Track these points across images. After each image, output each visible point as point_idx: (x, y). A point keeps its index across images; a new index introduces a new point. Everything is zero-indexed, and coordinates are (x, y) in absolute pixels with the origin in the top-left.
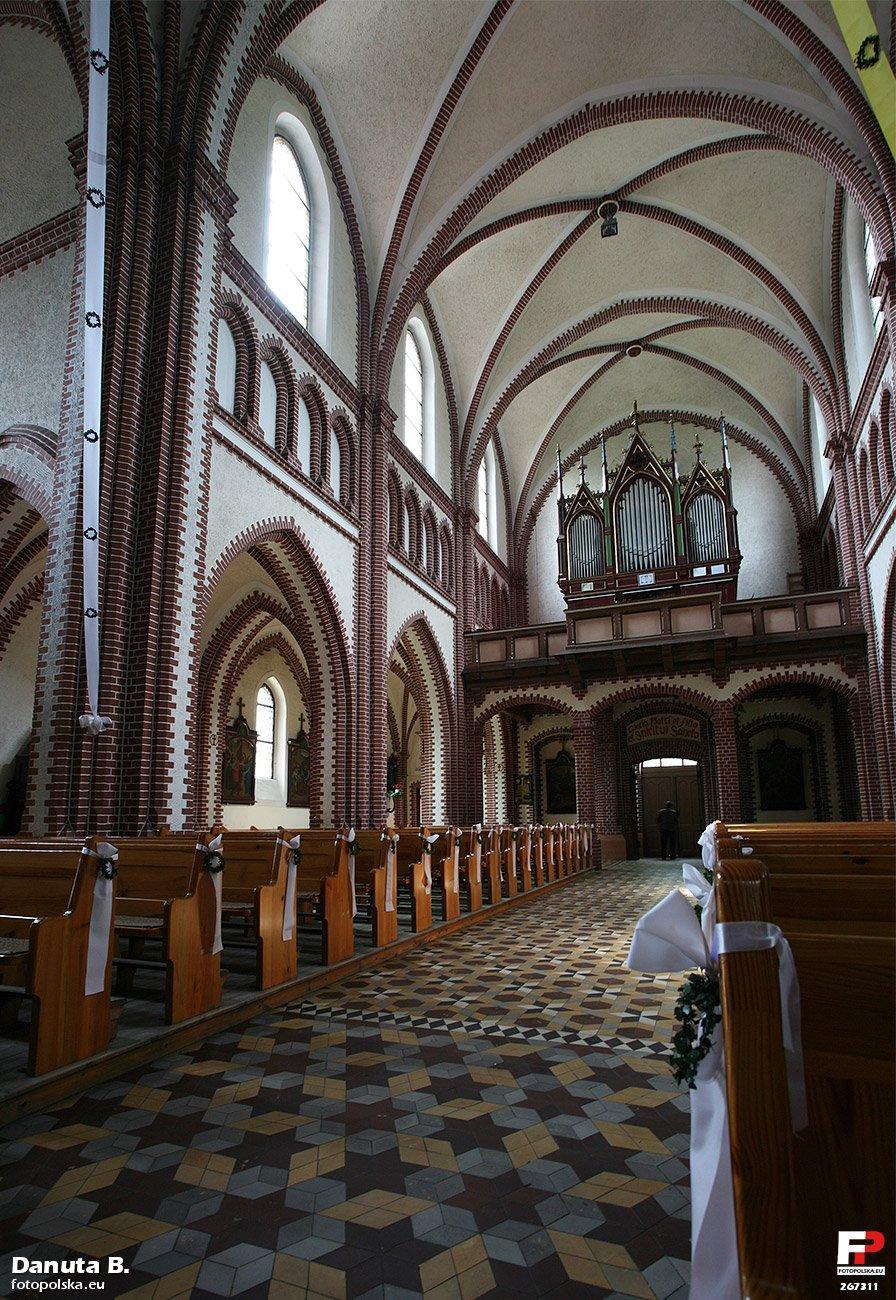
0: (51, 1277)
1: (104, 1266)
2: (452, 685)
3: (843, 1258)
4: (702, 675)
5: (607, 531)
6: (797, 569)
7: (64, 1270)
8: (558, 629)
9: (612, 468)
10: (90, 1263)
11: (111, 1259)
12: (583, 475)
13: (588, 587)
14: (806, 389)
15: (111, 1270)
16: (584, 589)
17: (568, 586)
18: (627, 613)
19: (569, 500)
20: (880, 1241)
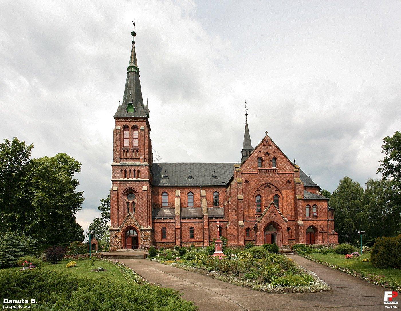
0: (14, 304)
1: (30, 301)
3: (386, 299)
7: (18, 302)
10: (26, 300)
11: (32, 299)
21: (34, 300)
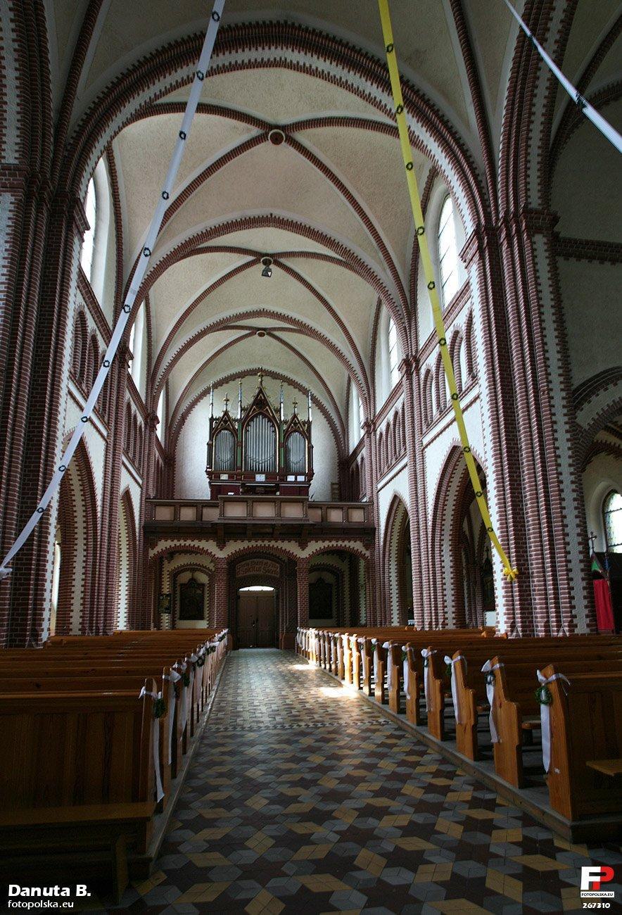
0: (35, 899)
1: (73, 891)
2: (137, 534)
3: (585, 885)
4: (293, 542)
5: (239, 446)
6: (336, 481)
7: (45, 894)
8: (199, 505)
9: (245, 405)
10: (63, 889)
11: (78, 886)
12: (227, 405)
13: (224, 477)
14: (349, 378)
15: (78, 894)
16: (222, 478)
17: (213, 475)
18: (256, 501)
19: (216, 419)
20: (611, 873)
21: (85, 887)
